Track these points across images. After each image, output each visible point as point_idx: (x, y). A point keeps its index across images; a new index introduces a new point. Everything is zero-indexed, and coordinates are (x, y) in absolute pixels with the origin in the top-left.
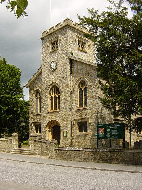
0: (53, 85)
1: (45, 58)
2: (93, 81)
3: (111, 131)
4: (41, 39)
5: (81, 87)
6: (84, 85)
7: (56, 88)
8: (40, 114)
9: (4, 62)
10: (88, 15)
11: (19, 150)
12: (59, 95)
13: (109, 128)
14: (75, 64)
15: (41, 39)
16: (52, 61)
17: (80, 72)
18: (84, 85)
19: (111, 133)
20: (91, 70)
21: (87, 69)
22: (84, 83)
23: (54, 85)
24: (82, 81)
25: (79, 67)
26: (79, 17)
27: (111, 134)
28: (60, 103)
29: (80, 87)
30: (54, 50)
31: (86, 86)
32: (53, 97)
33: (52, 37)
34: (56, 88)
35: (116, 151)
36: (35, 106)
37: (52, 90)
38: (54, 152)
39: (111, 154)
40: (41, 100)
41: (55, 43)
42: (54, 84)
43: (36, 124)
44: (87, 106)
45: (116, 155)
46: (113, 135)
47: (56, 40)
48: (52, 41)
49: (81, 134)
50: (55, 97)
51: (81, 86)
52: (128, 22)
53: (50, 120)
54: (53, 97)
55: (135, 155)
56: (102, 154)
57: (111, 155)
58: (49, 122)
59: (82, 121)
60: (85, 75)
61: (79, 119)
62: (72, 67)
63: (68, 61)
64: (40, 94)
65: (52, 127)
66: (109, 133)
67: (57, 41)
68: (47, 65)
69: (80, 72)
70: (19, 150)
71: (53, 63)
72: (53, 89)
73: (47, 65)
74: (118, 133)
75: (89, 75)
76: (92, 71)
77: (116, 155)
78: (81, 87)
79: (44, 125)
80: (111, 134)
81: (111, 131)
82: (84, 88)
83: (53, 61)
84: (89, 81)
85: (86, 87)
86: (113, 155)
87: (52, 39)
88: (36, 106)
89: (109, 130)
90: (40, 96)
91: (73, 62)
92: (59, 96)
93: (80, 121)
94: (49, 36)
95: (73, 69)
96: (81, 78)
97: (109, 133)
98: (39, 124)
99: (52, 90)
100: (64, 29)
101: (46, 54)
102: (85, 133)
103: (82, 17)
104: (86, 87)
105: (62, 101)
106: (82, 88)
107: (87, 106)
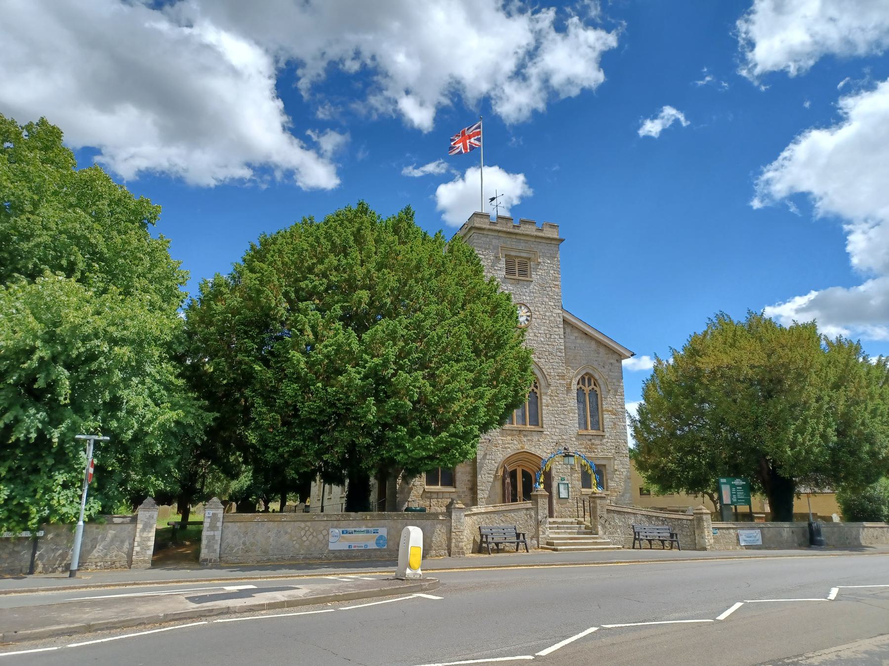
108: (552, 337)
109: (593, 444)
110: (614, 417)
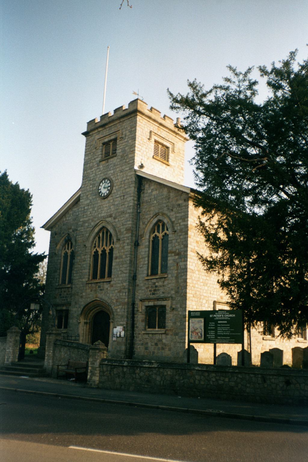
0: (100, 226)
1: (89, 171)
2: (180, 221)
3: (216, 326)
4: (83, 134)
5: (156, 233)
6: (163, 230)
7: (107, 233)
8: (69, 286)
9: (5, 175)
10: (187, 92)
11: (20, 365)
12: (112, 247)
13: (213, 319)
14: (147, 186)
15: (83, 134)
16: (101, 178)
17: (155, 202)
18: (163, 230)
19: (216, 330)
20: (177, 200)
21: (169, 199)
22: (163, 225)
23: (103, 227)
24: (159, 221)
25: (154, 193)
26: (171, 94)
27: (216, 332)
28: (114, 264)
29: (154, 232)
30: (108, 157)
31: (166, 231)
32: (100, 252)
33: (106, 132)
34: (107, 233)
35: (227, 370)
36: (60, 269)
37: (99, 238)
38: (97, 372)
39: (218, 378)
40: (74, 256)
41: (111, 143)
42: (103, 224)
43: (59, 308)
44: (166, 273)
45: (227, 380)
46: (220, 336)
47: (113, 137)
48: (106, 140)
49: (153, 332)
50: (104, 251)
51: (156, 231)
52: (257, 108)
53: (89, 300)
54: (100, 252)
55: (268, 382)
56: (197, 377)
57: (217, 380)
58: (87, 305)
59: (155, 304)
60: (165, 209)
61: (149, 300)
62: (140, 192)
63: (134, 179)
64: (72, 244)
65: (91, 314)
66: (212, 330)
67: (115, 140)
68: (91, 186)
69: (155, 202)
70: (20, 365)
71: (103, 182)
72: (101, 235)
73: (91, 186)
74: (232, 332)
75: (174, 210)
76: (180, 202)
77: (227, 380)
78: (156, 233)
79: (75, 310)
80: (216, 332)
81: (216, 326)
82: (163, 236)
83: (104, 179)
84: (61, 256)
85: (166, 234)
86: (222, 378)
87: (106, 135)
88: (61, 269)
89: (212, 324)
90: (71, 248)
91: (144, 182)
92: (111, 250)
93: (151, 304)
94: (100, 129)
95: (142, 195)
96: (156, 215)
97: (212, 330)
98: (64, 308)
99: (99, 238)
100: (129, 117)
101: (91, 165)
102: (163, 331)
103: (175, 95)
104: (166, 234)
105: (118, 260)
106: (157, 234)
107: (166, 273)
108: (125, 197)
109: (156, 286)
110: (177, 257)
